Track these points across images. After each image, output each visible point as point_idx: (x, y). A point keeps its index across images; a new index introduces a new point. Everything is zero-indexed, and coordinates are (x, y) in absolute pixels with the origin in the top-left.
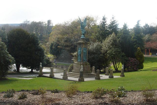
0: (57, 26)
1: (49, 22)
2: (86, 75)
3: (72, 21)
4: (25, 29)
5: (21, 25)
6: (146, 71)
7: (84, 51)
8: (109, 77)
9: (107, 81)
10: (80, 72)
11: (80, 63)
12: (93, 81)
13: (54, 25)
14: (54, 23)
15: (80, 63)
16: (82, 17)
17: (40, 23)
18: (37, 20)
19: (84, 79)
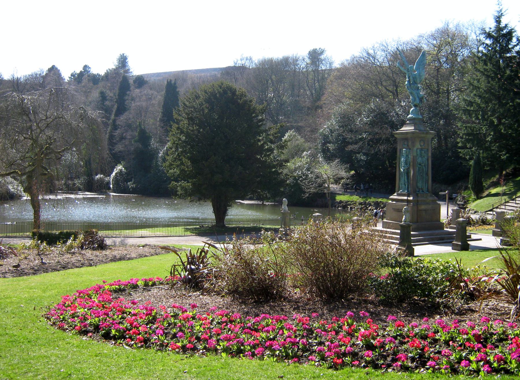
0: (343, 73)
1: (315, 56)
2: (430, 235)
3: (392, 47)
4: (239, 86)
5: (228, 72)
6: (484, 253)
7: (419, 160)
8: (501, 239)
9: (514, 251)
10: (400, 227)
11: (405, 198)
12: (445, 254)
13: (337, 65)
14: (339, 55)
15: (405, 198)
16: (440, 25)
17: (285, 61)
18: (277, 53)
19: (414, 247)
